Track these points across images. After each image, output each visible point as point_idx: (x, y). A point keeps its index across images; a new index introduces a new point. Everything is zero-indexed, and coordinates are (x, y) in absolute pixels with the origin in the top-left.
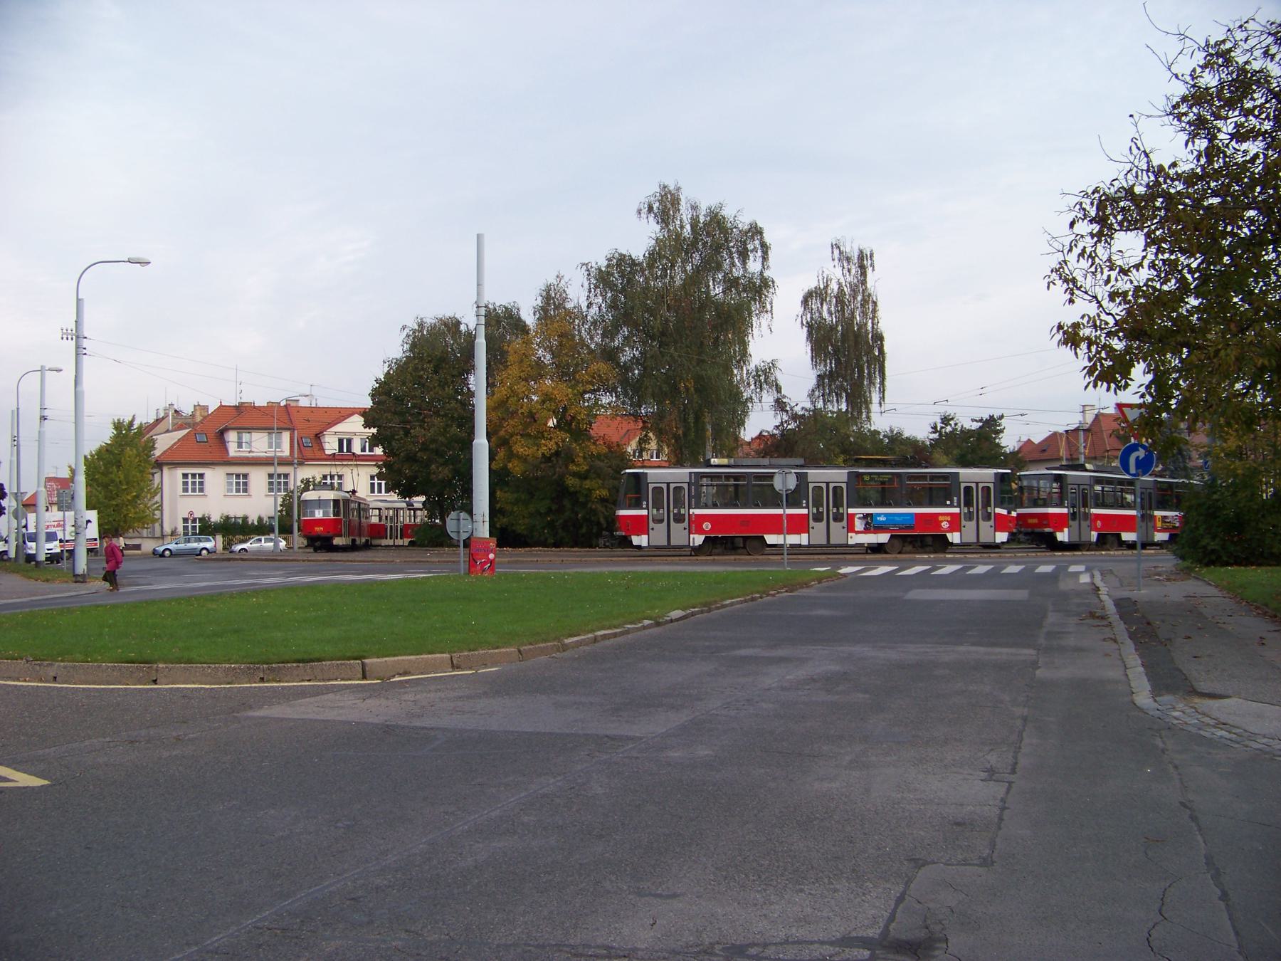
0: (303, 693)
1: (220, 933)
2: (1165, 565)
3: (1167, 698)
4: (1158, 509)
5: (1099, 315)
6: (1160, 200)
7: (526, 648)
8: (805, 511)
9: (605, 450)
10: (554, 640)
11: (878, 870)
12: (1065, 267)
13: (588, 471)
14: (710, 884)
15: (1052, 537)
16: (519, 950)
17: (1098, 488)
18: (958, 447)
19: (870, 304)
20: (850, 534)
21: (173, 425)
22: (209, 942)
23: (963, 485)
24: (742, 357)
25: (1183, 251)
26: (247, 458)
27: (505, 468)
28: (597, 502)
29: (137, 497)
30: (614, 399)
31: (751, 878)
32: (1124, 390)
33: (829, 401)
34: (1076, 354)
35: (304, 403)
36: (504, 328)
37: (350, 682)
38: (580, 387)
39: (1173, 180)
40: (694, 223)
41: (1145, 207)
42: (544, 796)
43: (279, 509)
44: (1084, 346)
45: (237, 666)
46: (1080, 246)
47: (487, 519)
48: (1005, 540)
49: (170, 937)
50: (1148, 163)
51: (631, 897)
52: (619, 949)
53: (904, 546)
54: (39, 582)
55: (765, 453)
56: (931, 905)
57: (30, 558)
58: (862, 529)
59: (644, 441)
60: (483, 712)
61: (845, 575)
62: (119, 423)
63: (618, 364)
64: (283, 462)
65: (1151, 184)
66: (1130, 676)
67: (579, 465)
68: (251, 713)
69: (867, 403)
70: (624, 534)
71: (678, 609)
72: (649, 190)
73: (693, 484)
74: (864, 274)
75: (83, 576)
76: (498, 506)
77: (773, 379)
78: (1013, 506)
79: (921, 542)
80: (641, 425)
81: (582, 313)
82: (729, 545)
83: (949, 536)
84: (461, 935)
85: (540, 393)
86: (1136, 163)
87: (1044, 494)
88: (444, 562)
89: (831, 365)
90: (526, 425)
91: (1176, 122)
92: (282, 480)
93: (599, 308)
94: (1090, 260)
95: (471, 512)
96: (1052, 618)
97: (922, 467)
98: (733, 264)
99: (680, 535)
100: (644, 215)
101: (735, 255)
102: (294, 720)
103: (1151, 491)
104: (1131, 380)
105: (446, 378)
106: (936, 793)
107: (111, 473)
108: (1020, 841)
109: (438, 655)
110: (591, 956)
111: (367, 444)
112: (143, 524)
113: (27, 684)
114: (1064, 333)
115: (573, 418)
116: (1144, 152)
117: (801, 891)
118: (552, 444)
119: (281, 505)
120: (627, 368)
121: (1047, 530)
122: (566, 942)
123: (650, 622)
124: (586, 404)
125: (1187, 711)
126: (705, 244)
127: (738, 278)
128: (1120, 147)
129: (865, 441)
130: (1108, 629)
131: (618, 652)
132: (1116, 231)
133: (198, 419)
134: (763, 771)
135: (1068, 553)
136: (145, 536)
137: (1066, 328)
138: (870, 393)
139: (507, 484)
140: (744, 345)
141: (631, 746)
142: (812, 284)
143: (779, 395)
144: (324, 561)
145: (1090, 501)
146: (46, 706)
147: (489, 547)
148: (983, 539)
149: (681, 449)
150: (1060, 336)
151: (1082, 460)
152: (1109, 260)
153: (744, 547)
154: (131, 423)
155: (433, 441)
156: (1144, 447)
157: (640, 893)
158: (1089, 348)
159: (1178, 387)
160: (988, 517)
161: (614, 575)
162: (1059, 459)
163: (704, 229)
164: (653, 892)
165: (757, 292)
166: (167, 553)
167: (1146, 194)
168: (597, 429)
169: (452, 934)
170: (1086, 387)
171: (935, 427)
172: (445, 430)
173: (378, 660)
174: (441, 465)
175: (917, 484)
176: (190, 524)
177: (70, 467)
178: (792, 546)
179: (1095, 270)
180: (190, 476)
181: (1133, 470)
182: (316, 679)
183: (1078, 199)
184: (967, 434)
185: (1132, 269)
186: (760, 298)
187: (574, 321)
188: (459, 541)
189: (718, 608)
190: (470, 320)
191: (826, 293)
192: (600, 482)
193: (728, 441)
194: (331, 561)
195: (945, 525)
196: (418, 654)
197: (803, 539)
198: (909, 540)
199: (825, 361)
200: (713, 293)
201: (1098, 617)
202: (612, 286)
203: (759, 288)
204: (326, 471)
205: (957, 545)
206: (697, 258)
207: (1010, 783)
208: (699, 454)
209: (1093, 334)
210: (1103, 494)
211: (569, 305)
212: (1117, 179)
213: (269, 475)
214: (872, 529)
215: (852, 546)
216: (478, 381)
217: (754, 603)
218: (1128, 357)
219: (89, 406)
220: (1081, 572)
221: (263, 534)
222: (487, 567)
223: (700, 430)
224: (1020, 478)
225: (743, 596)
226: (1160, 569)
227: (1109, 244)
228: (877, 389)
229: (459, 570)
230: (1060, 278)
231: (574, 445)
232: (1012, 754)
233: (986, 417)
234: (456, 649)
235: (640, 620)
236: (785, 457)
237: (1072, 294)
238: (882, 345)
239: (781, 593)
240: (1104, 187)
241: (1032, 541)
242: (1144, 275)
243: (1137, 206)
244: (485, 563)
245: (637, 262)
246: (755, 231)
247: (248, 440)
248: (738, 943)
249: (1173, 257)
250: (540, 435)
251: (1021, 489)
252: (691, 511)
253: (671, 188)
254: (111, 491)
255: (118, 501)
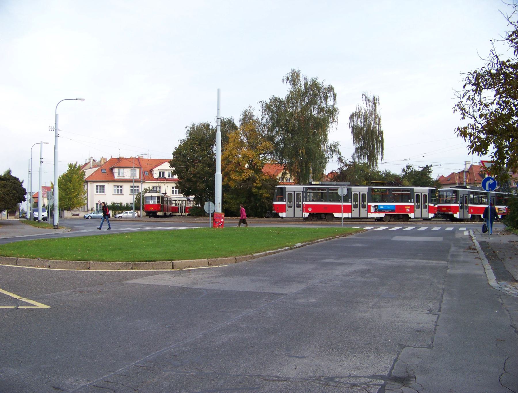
0: (148, 274)
1: (122, 368)
2: (499, 228)
3: (503, 282)
4: (497, 205)
5: (475, 124)
6: (502, 76)
7: (238, 257)
8: (350, 204)
9: (268, 177)
10: (250, 254)
11: (386, 349)
12: (461, 104)
13: (261, 186)
14: (318, 353)
15: (452, 216)
16: (242, 377)
17: (472, 196)
18: (413, 178)
19: (378, 119)
20: (369, 213)
21: (93, 166)
22: (118, 371)
23: (415, 194)
24: (325, 140)
25: (510, 97)
26: (122, 179)
27: (228, 184)
28: (265, 199)
29: (78, 194)
30: (272, 157)
31: (335, 351)
32: (485, 155)
33: (360, 159)
34: (465, 140)
35: (145, 157)
36: (227, 127)
37: (167, 270)
38: (258, 152)
39: (508, 67)
40: (306, 85)
41: (495, 79)
42: (248, 316)
43: (135, 200)
44: (468, 136)
45: (122, 263)
46: (468, 95)
47: (221, 205)
48: (433, 217)
49: (102, 368)
50: (497, 60)
51: (286, 357)
52: (282, 378)
53: (391, 219)
54: (40, 228)
55: (334, 180)
56: (408, 363)
57: (35, 219)
58: (374, 211)
59: (284, 174)
60: (222, 283)
61: (367, 230)
62: (71, 165)
63: (274, 143)
64: (137, 181)
65: (498, 69)
66: (487, 273)
67: (258, 184)
68: (128, 282)
69: (376, 160)
70: (276, 212)
71: (299, 243)
72: (287, 71)
73: (305, 192)
74: (375, 106)
75: (57, 226)
76: (224, 200)
77: (337, 149)
78: (436, 203)
79: (398, 217)
80: (283, 167)
81: (259, 121)
82: (319, 217)
83: (409, 214)
84: (218, 371)
85: (242, 154)
86: (492, 60)
87: (449, 198)
88: (202, 222)
89: (361, 144)
90: (236, 167)
91: (510, 43)
92: (136, 189)
93: (266, 119)
94: (472, 101)
95: (214, 202)
96: (453, 249)
97: (399, 186)
98: (322, 102)
99: (299, 213)
100: (285, 81)
101: (323, 98)
102: (146, 285)
103: (494, 197)
104: (488, 151)
105: (204, 148)
106: (408, 318)
107: (68, 185)
108: (444, 339)
109: (203, 260)
110: (271, 380)
111: (171, 174)
112: (80, 205)
113: (39, 268)
114: (460, 131)
115: (255, 164)
116: (496, 56)
117: (355, 356)
118: (247, 175)
119: (136, 199)
120: (277, 144)
121: (450, 213)
122: (261, 375)
123: (288, 248)
124: (261, 159)
125: (511, 288)
126: (310, 94)
127: (323, 108)
128: (486, 54)
129: (375, 175)
130: (477, 254)
131: (275, 259)
132: (483, 89)
133: (103, 163)
134: (337, 308)
135: (459, 223)
136: (81, 210)
137: (461, 129)
138: (377, 156)
139: (228, 191)
140: (326, 135)
141: (283, 297)
142: (354, 110)
143: (340, 156)
144: (154, 221)
145: (468, 201)
146: (47, 277)
147: (221, 217)
148: (423, 216)
149: (299, 178)
150: (458, 132)
151: (465, 184)
152: (480, 101)
153: (325, 218)
154: (76, 165)
155: (198, 173)
156: (492, 179)
157: (290, 356)
158: (470, 138)
159: (508, 154)
160: (425, 207)
161: (272, 228)
162: (455, 184)
163: (310, 87)
164: (295, 356)
165: (331, 113)
166: (90, 217)
167: (496, 73)
168: (265, 169)
169: (215, 370)
170: (469, 153)
171: (404, 170)
172: (203, 169)
173: (179, 261)
174: (201, 183)
175: (396, 193)
176: (99, 206)
177: (51, 182)
178: (345, 218)
179: (474, 104)
180: (99, 186)
181: (487, 188)
182: (153, 268)
183: (467, 76)
184: (417, 173)
185: (489, 105)
186: (333, 116)
187: (256, 125)
188: (209, 214)
189: (315, 243)
190: (213, 124)
191: (360, 114)
192: (266, 191)
193: (318, 174)
194: (156, 221)
195: (408, 210)
196: (194, 259)
197: (349, 215)
198: (393, 216)
199: (359, 142)
200: (313, 114)
201: (472, 249)
202: (272, 111)
203: (332, 112)
204: (154, 185)
205: (413, 219)
206: (307, 99)
207: (439, 315)
208: (307, 179)
209: (473, 132)
210: (474, 198)
211: (254, 118)
212: (484, 67)
213: (131, 186)
214: (378, 211)
215: (369, 218)
216: (217, 149)
217: (330, 241)
218: (487, 142)
219: (60, 158)
220: (464, 231)
221: (128, 210)
222: (220, 224)
223: (308, 170)
224: (439, 191)
225: (326, 238)
226: (498, 230)
227: (480, 94)
228: (380, 154)
229: (209, 226)
230: (459, 108)
231: (256, 175)
232: (439, 304)
233: (425, 166)
234: (210, 257)
235: (284, 247)
236: (342, 181)
237: (464, 115)
238: (382, 136)
239: (341, 237)
240: (479, 71)
241: (444, 217)
242: (494, 107)
243: (492, 78)
244: (220, 223)
245: (282, 101)
246: (331, 88)
247: (122, 172)
248: (331, 376)
249: (507, 100)
250: (242, 171)
251: (439, 196)
252: (304, 203)
253: (296, 71)
254: (68, 192)
255: (70, 196)
